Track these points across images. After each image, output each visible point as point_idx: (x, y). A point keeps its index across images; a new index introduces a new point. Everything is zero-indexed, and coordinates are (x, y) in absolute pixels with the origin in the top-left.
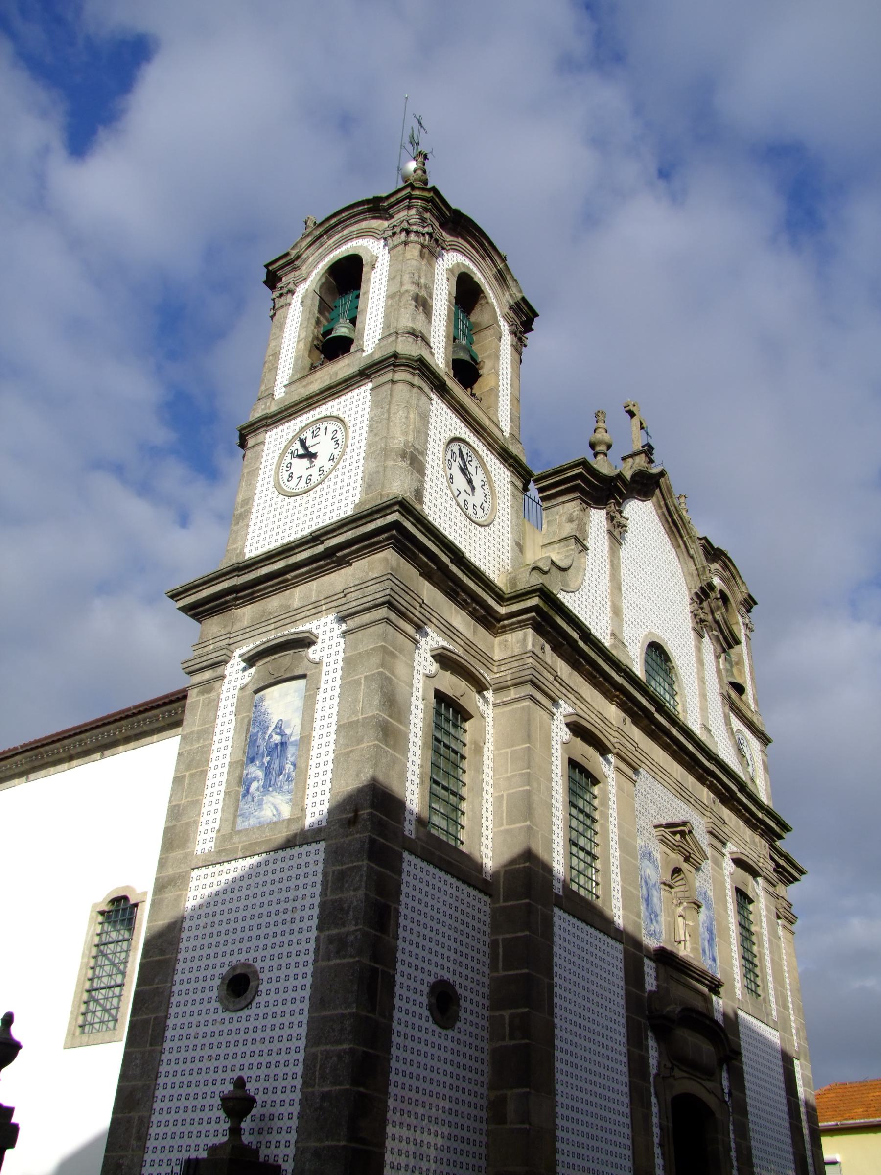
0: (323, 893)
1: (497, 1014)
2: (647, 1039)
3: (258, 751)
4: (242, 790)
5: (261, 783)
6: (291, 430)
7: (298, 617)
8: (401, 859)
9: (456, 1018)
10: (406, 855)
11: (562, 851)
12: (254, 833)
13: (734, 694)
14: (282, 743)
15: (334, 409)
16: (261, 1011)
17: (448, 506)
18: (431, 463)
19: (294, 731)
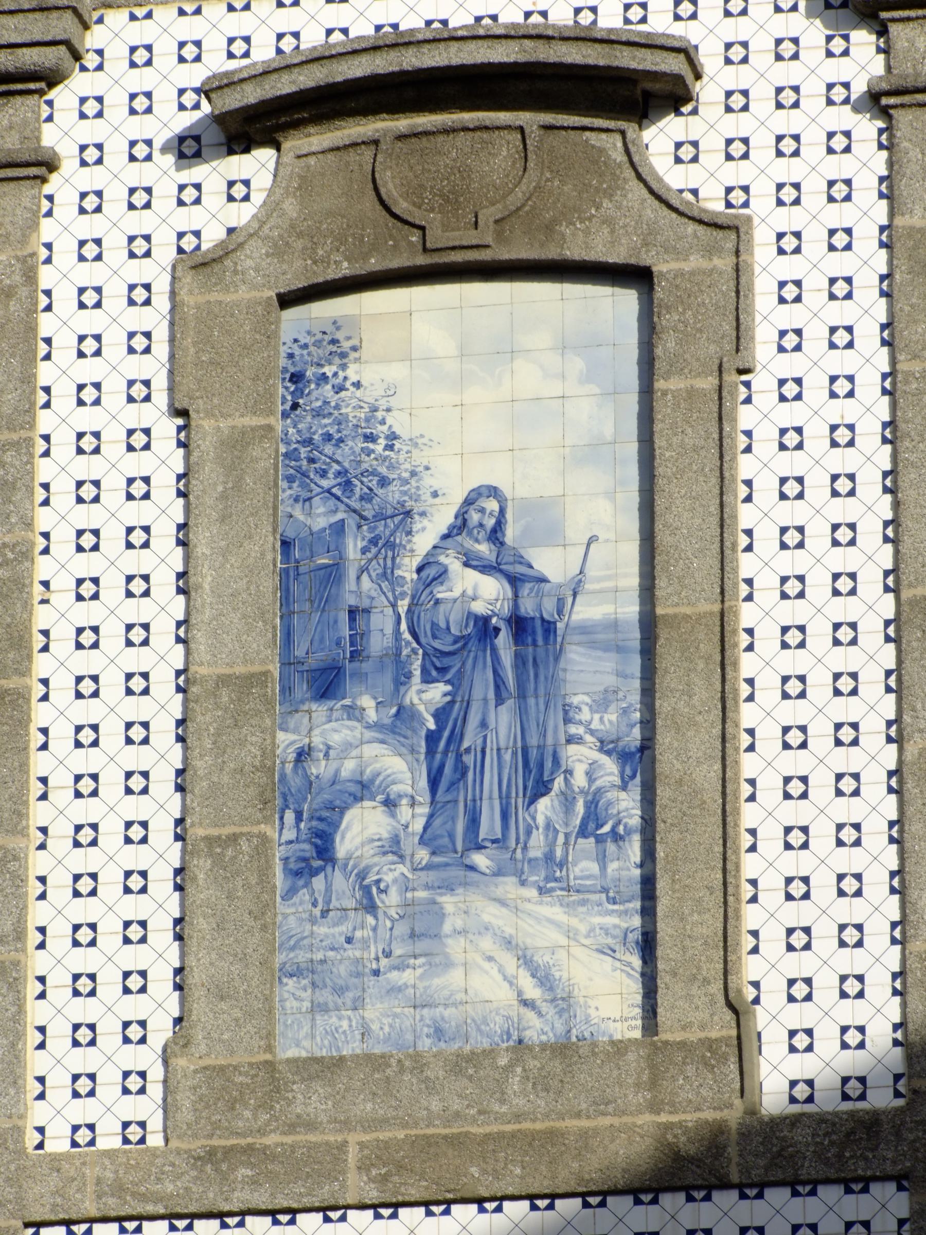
3: (358, 639)
4: (285, 836)
5: (414, 817)
12: (430, 1086)
19: (589, 548)
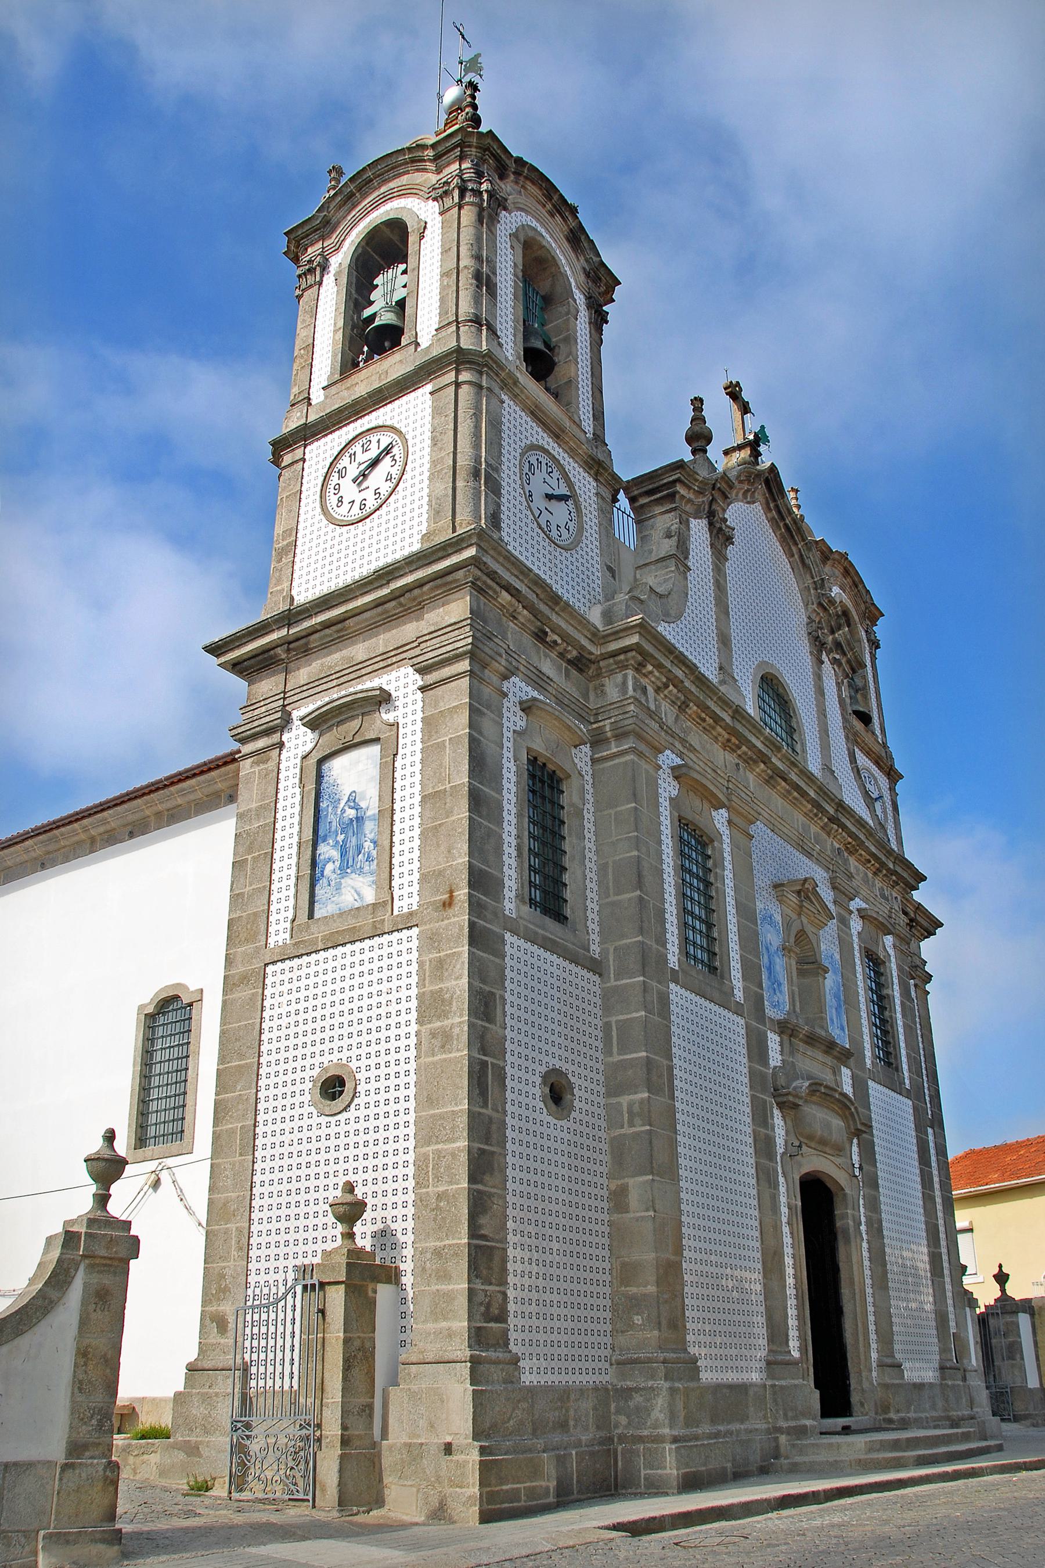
0: (421, 984)
1: (613, 1100)
2: (772, 1117)
5: (337, 864)
6: (335, 444)
7: (363, 672)
8: (503, 941)
9: (572, 1108)
10: (508, 936)
11: (675, 922)
13: (858, 725)
14: (357, 818)
15: (388, 417)
16: (362, 1113)
17: (529, 530)
18: (507, 480)
19: (371, 803)
